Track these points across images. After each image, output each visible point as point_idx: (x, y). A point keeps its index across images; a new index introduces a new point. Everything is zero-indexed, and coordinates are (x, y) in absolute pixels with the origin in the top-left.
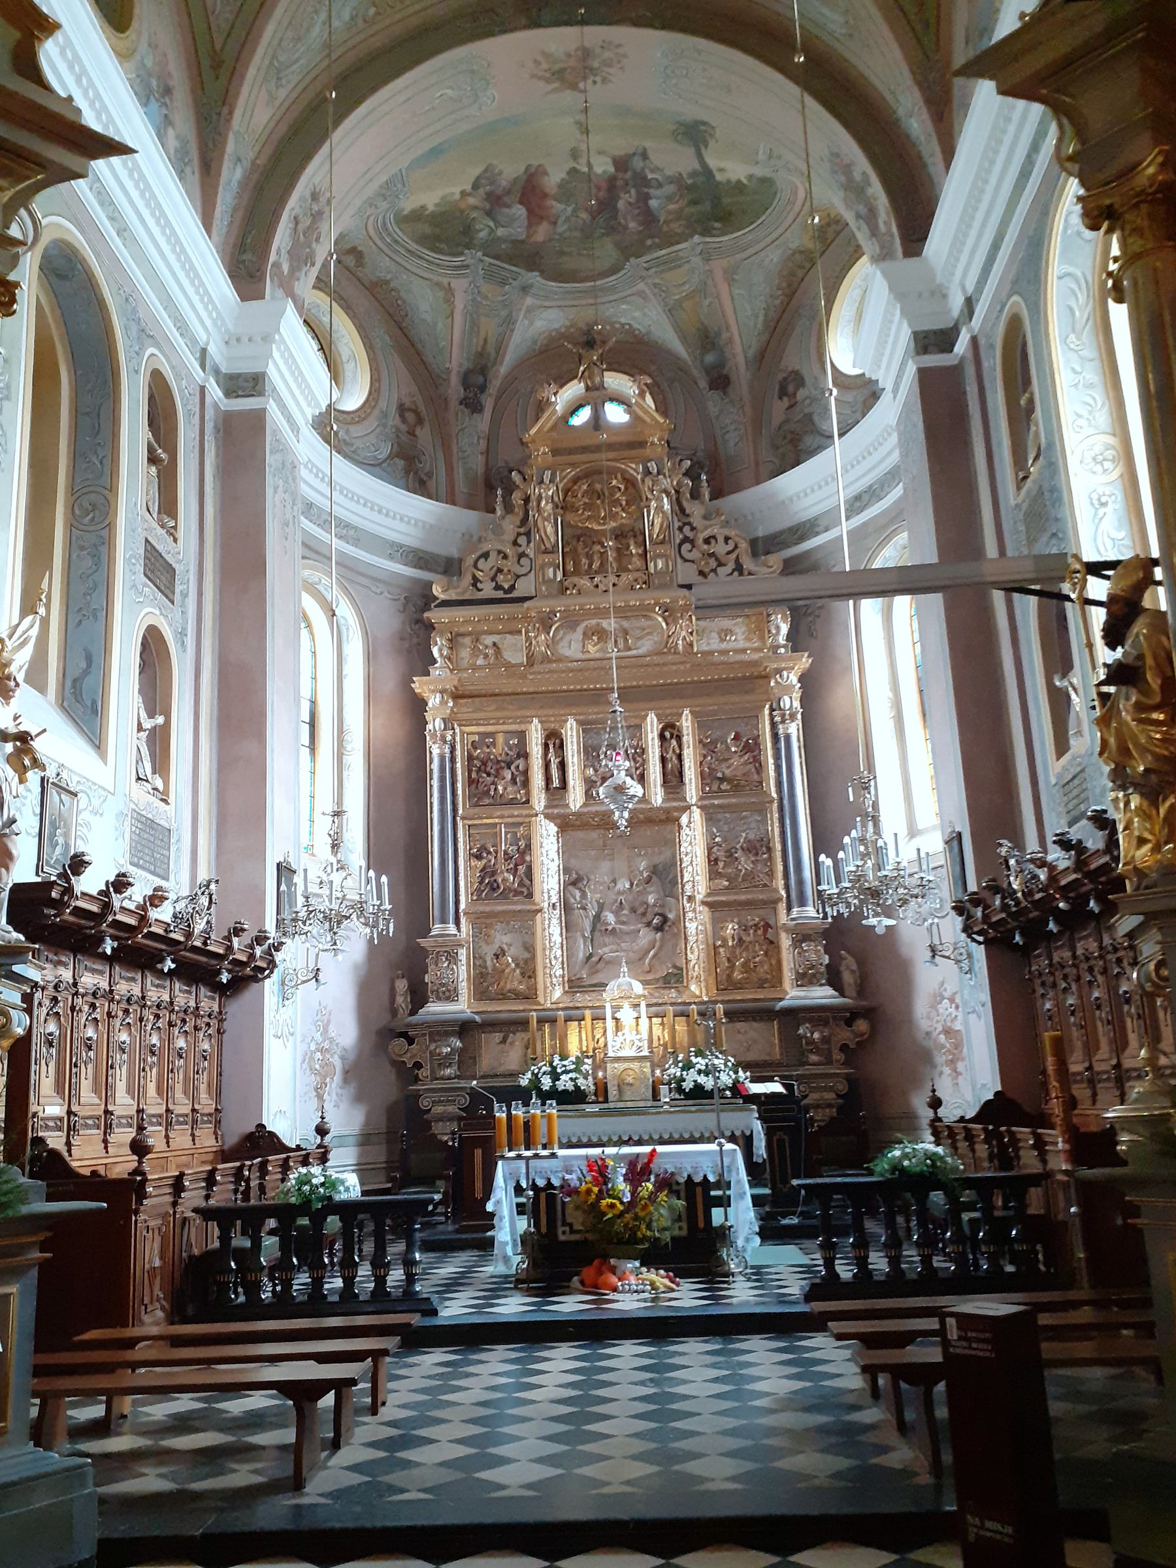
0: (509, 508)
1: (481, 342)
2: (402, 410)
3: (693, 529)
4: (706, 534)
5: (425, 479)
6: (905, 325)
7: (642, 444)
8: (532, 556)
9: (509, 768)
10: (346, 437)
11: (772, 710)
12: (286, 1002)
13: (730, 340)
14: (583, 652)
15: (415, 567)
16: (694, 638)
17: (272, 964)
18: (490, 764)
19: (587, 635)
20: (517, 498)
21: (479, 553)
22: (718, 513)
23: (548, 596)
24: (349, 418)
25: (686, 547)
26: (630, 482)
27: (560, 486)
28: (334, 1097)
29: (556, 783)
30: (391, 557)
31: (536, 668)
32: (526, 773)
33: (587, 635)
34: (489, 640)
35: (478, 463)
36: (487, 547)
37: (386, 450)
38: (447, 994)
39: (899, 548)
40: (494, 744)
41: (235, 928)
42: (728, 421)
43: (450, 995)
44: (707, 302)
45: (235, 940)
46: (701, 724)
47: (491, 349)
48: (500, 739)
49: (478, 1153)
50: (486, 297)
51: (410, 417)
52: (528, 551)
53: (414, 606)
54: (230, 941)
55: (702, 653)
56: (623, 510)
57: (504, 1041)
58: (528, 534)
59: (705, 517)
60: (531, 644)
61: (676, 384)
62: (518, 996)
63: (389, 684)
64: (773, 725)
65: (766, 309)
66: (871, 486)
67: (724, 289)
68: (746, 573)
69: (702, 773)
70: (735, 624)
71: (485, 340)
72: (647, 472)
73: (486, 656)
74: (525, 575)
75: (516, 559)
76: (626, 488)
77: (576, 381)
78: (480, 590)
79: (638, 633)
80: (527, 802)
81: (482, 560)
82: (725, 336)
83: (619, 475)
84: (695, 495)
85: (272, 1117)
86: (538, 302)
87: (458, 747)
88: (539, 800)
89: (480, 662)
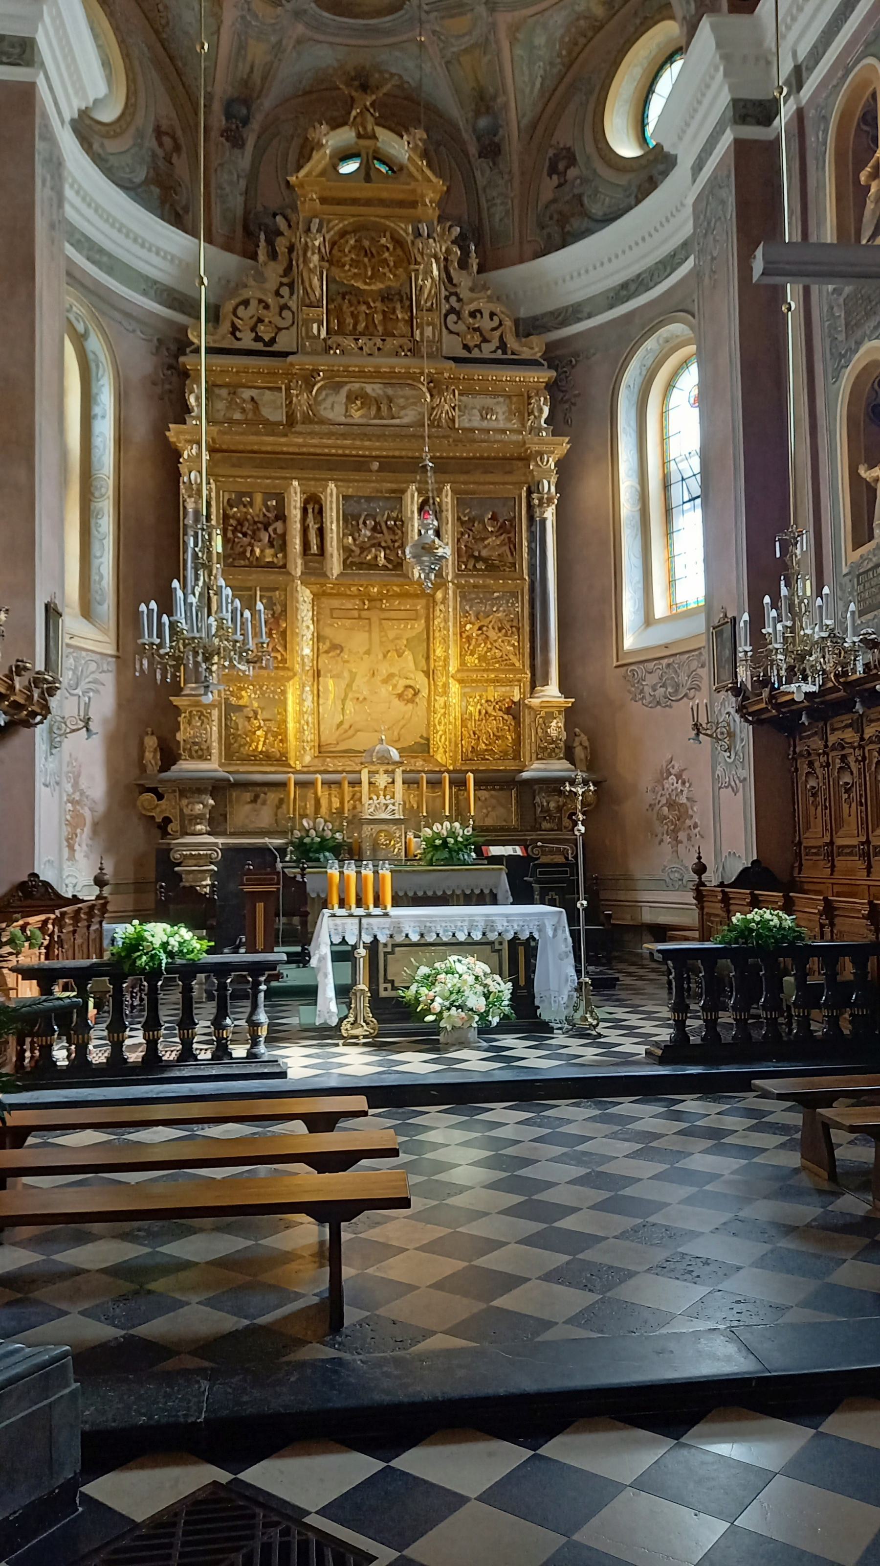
0: (273, 255)
1: (247, 69)
2: (159, 133)
3: (459, 300)
4: (473, 307)
5: (181, 212)
6: (726, 89)
7: (413, 204)
8: (294, 309)
9: (266, 529)
10: (100, 151)
11: (529, 492)
12: (54, 751)
13: (506, 106)
14: (346, 416)
15: (170, 307)
16: (457, 413)
17: (46, 710)
18: (247, 524)
19: (351, 398)
20: (281, 244)
21: (237, 300)
22: (485, 287)
23: (314, 353)
24: (103, 129)
25: (452, 318)
26: (398, 242)
27: (327, 237)
28: (85, 848)
29: (314, 549)
30: (145, 293)
31: (299, 428)
32: (283, 537)
33: (351, 398)
34: (247, 394)
35: (237, 202)
36: (247, 294)
37: (140, 175)
38: (200, 753)
39: (661, 341)
40: (251, 504)
41: (17, 667)
42: (495, 194)
43: (203, 755)
44: (485, 60)
45: (17, 679)
46: (460, 502)
47: (257, 77)
48: (258, 498)
49: (260, 906)
50: (256, 16)
51: (167, 140)
52: (290, 304)
53: (168, 349)
54: (12, 680)
55: (464, 429)
56: (390, 271)
57: (254, 800)
58: (291, 285)
59: (472, 290)
60: (291, 402)
61: (442, 148)
62: (268, 758)
63: (141, 430)
64: (530, 507)
65: (543, 79)
66: (639, 275)
67: (505, 45)
68: (509, 352)
69: (459, 549)
70: (498, 403)
71: (252, 67)
72: (418, 234)
73: (243, 410)
74: (287, 328)
75: (277, 310)
76: (394, 249)
77: (346, 128)
78: (238, 339)
79: (401, 401)
80: (284, 566)
81: (242, 308)
82: (500, 100)
83: (388, 234)
84: (463, 264)
85: (42, 867)
86: (309, 33)
87: (213, 503)
88: (297, 567)
89: (237, 416)
